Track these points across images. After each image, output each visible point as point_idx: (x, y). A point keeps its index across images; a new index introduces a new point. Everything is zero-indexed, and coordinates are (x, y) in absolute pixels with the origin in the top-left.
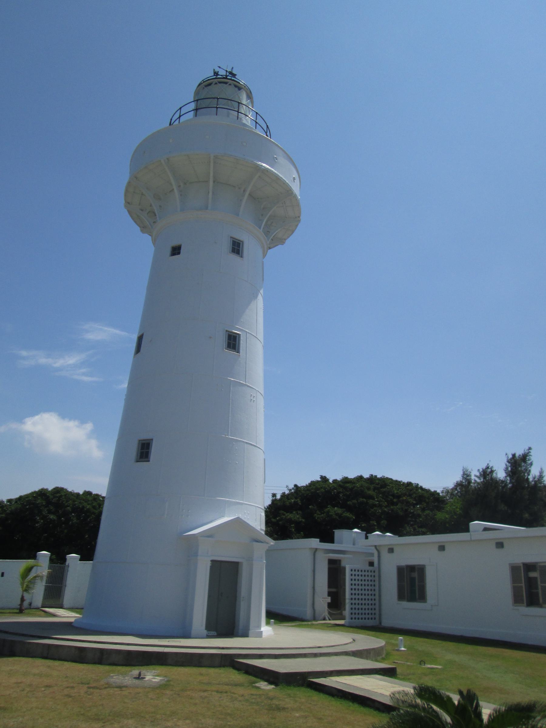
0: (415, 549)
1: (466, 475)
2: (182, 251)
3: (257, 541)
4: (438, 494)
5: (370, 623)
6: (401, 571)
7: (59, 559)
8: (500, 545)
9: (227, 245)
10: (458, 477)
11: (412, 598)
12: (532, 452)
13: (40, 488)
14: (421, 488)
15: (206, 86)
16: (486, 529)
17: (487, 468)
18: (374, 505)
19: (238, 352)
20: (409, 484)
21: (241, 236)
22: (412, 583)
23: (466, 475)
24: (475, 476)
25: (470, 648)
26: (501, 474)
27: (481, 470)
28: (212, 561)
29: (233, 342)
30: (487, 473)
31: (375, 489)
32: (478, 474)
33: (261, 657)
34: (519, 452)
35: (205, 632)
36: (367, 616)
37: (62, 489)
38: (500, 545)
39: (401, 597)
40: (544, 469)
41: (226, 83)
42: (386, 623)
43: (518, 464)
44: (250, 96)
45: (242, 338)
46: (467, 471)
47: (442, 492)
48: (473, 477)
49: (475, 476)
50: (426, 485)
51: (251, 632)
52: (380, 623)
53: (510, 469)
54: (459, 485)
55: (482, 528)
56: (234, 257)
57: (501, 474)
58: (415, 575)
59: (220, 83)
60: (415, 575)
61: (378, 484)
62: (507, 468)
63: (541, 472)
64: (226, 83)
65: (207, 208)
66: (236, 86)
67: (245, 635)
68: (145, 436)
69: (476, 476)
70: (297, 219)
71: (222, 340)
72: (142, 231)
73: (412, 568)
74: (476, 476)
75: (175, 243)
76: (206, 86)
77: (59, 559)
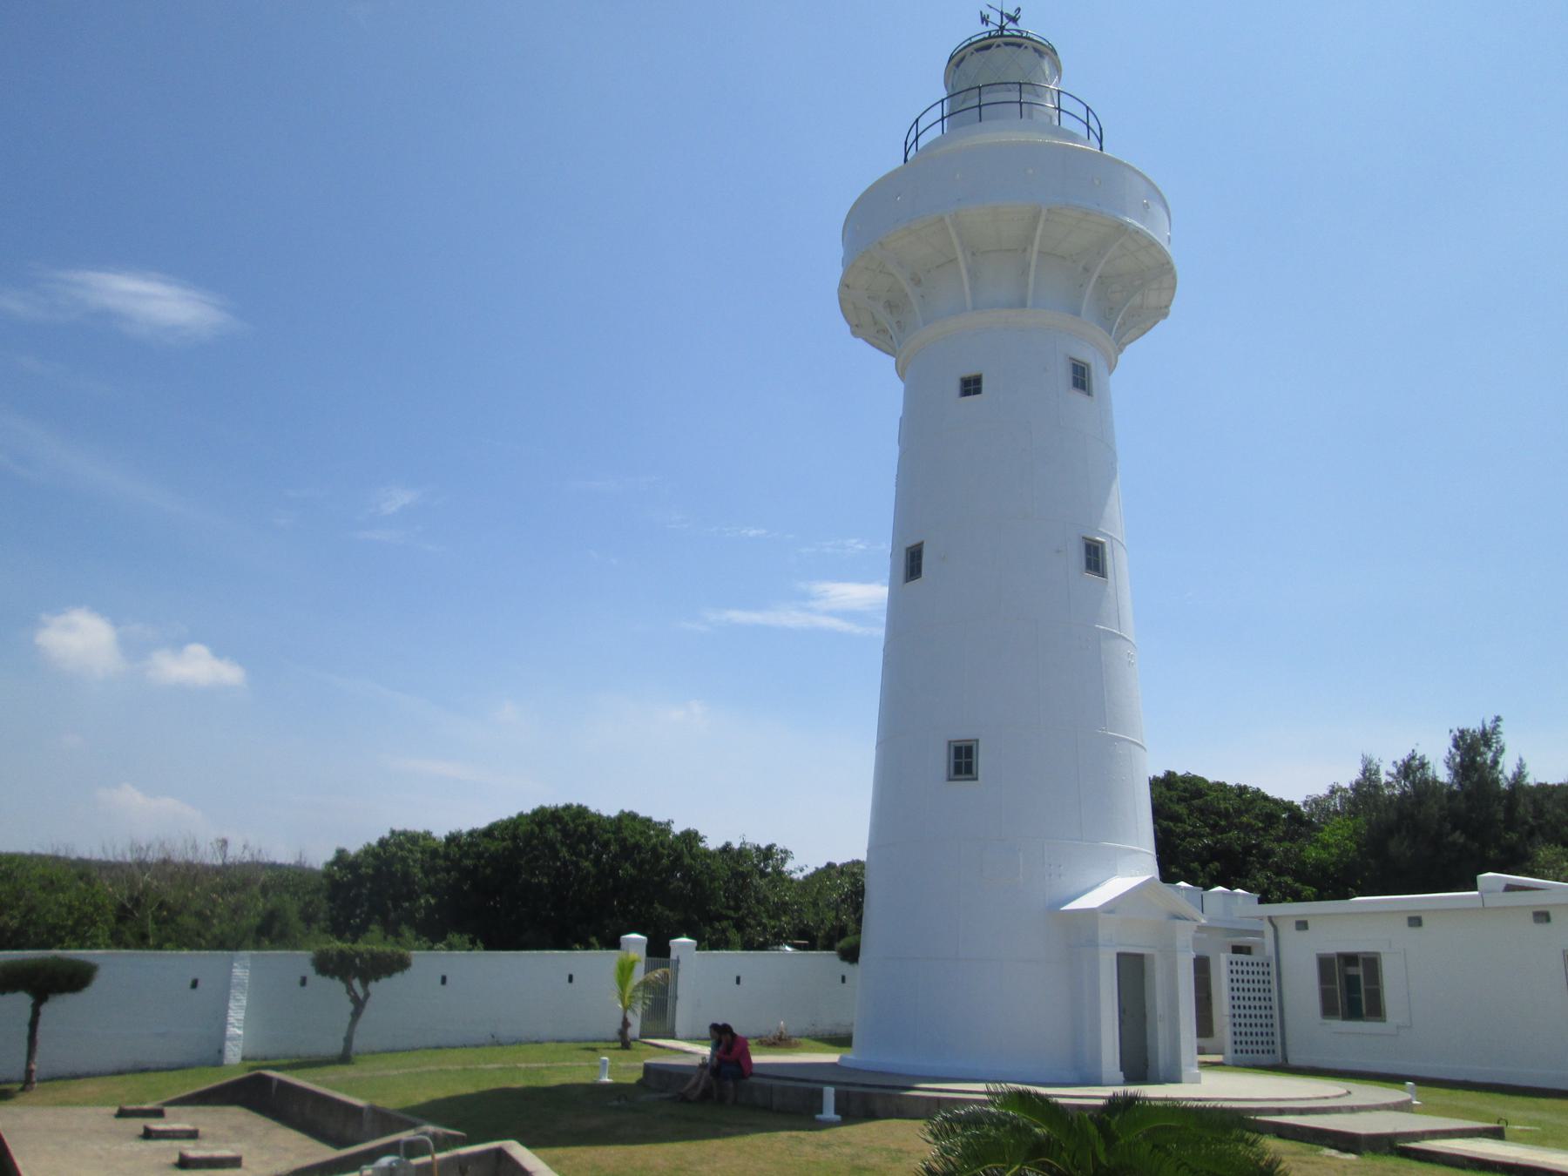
0: (1364, 921)
1: (1369, 772)
2: (984, 385)
3: (1177, 917)
4: (1298, 808)
5: (1266, 1059)
6: (1325, 963)
7: (658, 950)
8: (1542, 916)
9: (1065, 375)
10: (1348, 776)
11: (1353, 1011)
12: (1503, 727)
13: (536, 806)
14: (1266, 798)
15: (978, 50)
16: (1510, 888)
17: (1413, 758)
18: (1187, 834)
19: (1104, 575)
20: (1242, 790)
21: (1086, 355)
22: (1352, 987)
23: (1369, 772)
24: (1386, 772)
25: (1543, 1102)
26: (1443, 774)
27: (1400, 763)
28: (1119, 955)
29: (1094, 558)
30: (1411, 768)
31: (1181, 800)
32: (1394, 771)
33: (1281, 1112)
34: (1474, 725)
35: (1120, 1076)
36: (1260, 1048)
37: (633, 817)
38: (1542, 916)
39: (1329, 1010)
40: (1526, 760)
41: (1019, 46)
42: (1294, 1060)
43: (1473, 750)
44: (1057, 68)
45: (1108, 549)
46: (1370, 762)
47: (1305, 804)
48: (1384, 778)
49: (1386, 772)
50: (1273, 791)
51: (1184, 1076)
52: (1285, 1059)
53: (1458, 759)
54: (1357, 788)
55: (1502, 886)
56: (1078, 395)
57: (1443, 774)
58: (1359, 971)
59: (1007, 44)
60: (1359, 971)
61: (1185, 790)
62: (1453, 757)
63: (1521, 766)
64: (1019, 46)
65: (1023, 304)
66: (1036, 50)
67: (1175, 1078)
68: (963, 734)
69: (1388, 774)
70: (1162, 312)
71: (1077, 556)
72: (853, 333)
73: (1350, 959)
74: (1388, 774)
75: (970, 372)
76: (978, 50)
77: (658, 950)
